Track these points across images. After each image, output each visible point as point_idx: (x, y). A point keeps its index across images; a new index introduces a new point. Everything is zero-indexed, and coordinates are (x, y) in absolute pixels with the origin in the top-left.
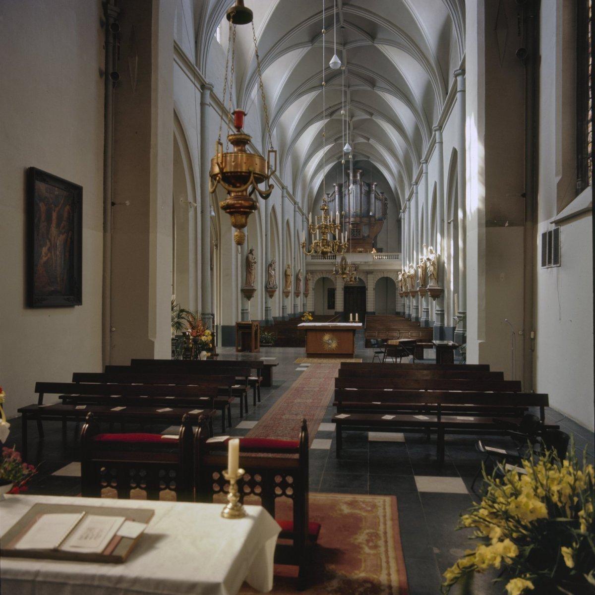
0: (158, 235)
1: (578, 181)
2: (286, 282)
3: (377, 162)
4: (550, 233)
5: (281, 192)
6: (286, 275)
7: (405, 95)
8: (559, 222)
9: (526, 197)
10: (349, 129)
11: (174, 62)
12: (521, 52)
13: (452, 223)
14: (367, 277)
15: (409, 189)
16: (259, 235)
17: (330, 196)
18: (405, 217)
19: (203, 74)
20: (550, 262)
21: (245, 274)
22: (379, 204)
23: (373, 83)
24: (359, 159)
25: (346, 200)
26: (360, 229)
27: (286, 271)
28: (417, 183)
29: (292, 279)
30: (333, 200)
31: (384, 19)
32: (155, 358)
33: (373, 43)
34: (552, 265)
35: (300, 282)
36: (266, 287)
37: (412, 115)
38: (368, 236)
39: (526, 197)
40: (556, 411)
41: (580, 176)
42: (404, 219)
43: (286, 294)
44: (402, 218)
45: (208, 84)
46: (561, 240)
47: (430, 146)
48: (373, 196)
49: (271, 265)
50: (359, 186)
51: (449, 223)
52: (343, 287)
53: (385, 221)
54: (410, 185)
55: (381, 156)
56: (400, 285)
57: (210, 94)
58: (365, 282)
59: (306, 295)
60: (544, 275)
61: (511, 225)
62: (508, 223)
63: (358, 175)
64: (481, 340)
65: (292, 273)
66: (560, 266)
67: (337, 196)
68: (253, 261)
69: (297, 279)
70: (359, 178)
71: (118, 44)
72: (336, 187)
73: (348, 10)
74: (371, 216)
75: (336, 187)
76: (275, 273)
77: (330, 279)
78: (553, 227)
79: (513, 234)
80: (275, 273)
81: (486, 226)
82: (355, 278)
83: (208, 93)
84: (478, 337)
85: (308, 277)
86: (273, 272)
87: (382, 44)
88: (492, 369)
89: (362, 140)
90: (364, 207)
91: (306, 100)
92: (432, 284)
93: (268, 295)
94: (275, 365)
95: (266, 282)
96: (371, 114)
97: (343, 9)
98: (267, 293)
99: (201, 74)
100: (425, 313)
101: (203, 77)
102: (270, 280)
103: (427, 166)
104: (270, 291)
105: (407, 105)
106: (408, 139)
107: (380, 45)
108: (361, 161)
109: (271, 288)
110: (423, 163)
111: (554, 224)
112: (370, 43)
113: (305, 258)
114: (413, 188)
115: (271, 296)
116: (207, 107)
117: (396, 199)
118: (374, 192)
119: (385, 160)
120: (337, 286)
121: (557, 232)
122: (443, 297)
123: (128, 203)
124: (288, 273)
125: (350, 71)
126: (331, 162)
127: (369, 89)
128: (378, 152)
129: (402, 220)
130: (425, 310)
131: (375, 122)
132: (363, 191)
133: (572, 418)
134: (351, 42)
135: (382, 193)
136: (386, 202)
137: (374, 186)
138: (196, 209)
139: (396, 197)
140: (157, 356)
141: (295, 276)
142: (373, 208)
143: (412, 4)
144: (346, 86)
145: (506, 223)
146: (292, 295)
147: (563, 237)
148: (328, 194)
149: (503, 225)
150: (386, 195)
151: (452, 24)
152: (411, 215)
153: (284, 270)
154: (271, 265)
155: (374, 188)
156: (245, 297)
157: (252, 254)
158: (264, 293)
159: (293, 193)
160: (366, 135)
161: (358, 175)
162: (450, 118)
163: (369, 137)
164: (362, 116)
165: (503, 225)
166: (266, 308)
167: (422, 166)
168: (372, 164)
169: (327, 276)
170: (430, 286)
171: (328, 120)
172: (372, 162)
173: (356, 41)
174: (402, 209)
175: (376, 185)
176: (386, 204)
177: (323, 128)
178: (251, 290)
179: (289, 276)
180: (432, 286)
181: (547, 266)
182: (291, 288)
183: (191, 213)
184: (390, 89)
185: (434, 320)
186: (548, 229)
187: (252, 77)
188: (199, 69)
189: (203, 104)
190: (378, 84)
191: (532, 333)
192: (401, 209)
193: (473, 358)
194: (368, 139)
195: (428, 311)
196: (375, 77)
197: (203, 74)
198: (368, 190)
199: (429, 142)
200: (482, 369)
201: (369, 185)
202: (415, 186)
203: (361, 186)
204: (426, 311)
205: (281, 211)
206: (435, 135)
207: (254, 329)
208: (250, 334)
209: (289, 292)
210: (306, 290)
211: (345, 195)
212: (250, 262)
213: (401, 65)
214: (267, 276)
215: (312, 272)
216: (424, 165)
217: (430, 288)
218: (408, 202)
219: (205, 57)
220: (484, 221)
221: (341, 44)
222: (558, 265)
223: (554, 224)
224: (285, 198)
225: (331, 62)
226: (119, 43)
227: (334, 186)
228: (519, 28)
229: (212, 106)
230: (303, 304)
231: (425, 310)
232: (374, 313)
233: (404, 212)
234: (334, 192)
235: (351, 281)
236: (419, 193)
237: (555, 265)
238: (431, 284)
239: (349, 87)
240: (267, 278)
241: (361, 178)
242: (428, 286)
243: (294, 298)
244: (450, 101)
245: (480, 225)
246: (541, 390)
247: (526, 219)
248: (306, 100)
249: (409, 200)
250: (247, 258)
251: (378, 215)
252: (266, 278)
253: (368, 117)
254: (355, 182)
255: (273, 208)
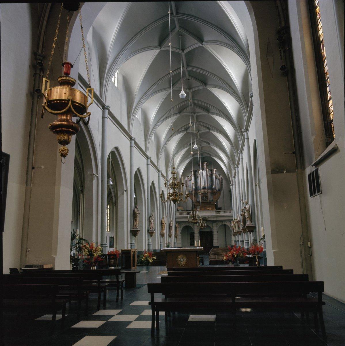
0: (62, 187)
1: (326, 138)
2: (162, 228)
3: (215, 157)
4: (313, 173)
5: (129, 142)
6: (162, 224)
7: (227, 116)
8: (317, 164)
9: (295, 154)
10: (197, 138)
11: (78, 85)
12: (283, 68)
13: (258, 185)
14: (213, 225)
15: (234, 170)
16: (143, 200)
17: (189, 178)
18: (233, 188)
19: (104, 101)
20: (315, 193)
21: (133, 220)
22: (218, 181)
23: (208, 111)
24: (205, 156)
25: (199, 180)
26: (207, 197)
27: (162, 221)
28: (238, 166)
29: (166, 226)
30: (191, 180)
31: (211, 73)
32: (57, 268)
33: (206, 87)
34: (317, 194)
35: (172, 228)
36: (148, 231)
37: (233, 129)
38: (213, 201)
39: (295, 154)
40: (331, 297)
41: (327, 134)
42: (233, 189)
43: (162, 235)
44: (232, 188)
45: (107, 106)
46: (320, 175)
47: (242, 141)
48: (214, 177)
49: (151, 217)
50: (206, 171)
51: (256, 185)
52: (199, 231)
53: (222, 191)
54: (234, 168)
55: (217, 153)
56: (232, 228)
57: (161, 174)
58: (212, 228)
59: (176, 237)
60: (313, 202)
61: (287, 172)
62: (286, 171)
63: (205, 165)
64: (275, 249)
65: (166, 221)
66: (321, 193)
67: (193, 178)
68: (137, 213)
69: (170, 227)
70: (205, 166)
71: (43, 74)
72: (192, 172)
73: (189, 68)
74: (213, 188)
75: (192, 172)
76: (108, 182)
77: (190, 226)
78: (314, 168)
79: (290, 178)
80: (108, 182)
81: (272, 173)
82: (204, 225)
83: (107, 111)
84: (273, 247)
85: (177, 225)
86: (152, 221)
87: (211, 87)
88: (284, 268)
89: (205, 144)
90: (209, 183)
91: (171, 121)
92: (248, 223)
93: (149, 235)
94: (137, 272)
95: (148, 227)
96: (209, 129)
97: (188, 68)
98: (149, 234)
99: (103, 101)
100: (247, 243)
101: (104, 102)
102: (150, 226)
103: (242, 155)
104: (151, 233)
105: (229, 122)
106: (232, 142)
107: (210, 88)
108: (207, 157)
109: (151, 231)
110: (239, 153)
111: (314, 167)
112: (204, 87)
113: (175, 214)
114: (236, 169)
115: (151, 236)
116: (106, 119)
117: (229, 181)
118: (215, 175)
119: (219, 155)
120: (195, 231)
121: (317, 171)
122: (256, 231)
123: (43, 167)
124: (163, 222)
125: (195, 104)
126: (188, 159)
127: (206, 114)
128: (215, 151)
129: (232, 190)
130: (247, 242)
131: (212, 133)
132: (208, 174)
133: (343, 301)
134: (193, 88)
135: (219, 175)
136: (222, 180)
137: (214, 171)
138: (98, 178)
139: (227, 176)
140: (58, 267)
141: (169, 225)
142: (214, 183)
143: (229, 69)
144: (193, 113)
145: (284, 171)
146: (166, 236)
147: (320, 174)
148: (188, 177)
149: (282, 172)
150: (221, 176)
151: (249, 76)
152: (236, 186)
153: (161, 220)
154: (151, 217)
155: (214, 172)
156: (132, 235)
157: (137, 209)
158: (147, 234)
159: (166, 175)
160: (207, 141)
161: (205, 165)
162: (251, 125)
163: (209, 142)
164: (204, 130)
165: (282, 172)
166: (148, 243)
167: (239, 155)
168: (213, 158)
169: (189, 225)
170: (247, 225)
171: (185, 133)
172: (213, 157)
173: (196, 87)
174: (231, 183)
175: (215, 171)
176: (222, 181)
177: (172, 125)
178: (137, 230)
179: (164, 224)
180: (249, 225)
181: (313, 196)
182: (166, 231)
183: (95, 182)
184: (219, 113)
185: (209, 195)
186: (311, 171)
187: (136, 107)
188: (102, 98)
189: (103, 118)
190: (211, 111)
191: (309, 243)
192: (231, 183)
193: (271, 262)
194: (209, 144)
195: (249, 242)
196: (208, 106)
197: (104, 101)
198: (211, 173)
199: (242, 139)
200: (277, 269)
201: (212, 171)
202: (236, 168)
203: (207, 171)
204: (247, 242)
205: (158, 185)
206: (244, 134)
207: (132, 254)
208: (130, 257)
209: (164, 234)
210: (176, 233)
211: (198, 177)
212: (135, 213)
213: (222, 98)
214: (149, 223)
215: (180, 223)
216: (240, 154)
217: (247, 226)
218: (234, 179)
219: (106, 90)
220: (270, 170)
221: (188, 89)
222: (320, 193)
223: (314, 167)
224: (133, 148)
225: (180, 94)
226: (43, 74)
227: (191, 172)
228: (281, 55)
229: (109, 118)
230: (175, 242)
231: (247, 242)
232: (218, 247)
233: (232, 185)
234: (192, 175)
235: (202, 226)
236: (239, 171)
237: (318, 194)
238: (248, 223)
239: (195, 113)
240: (149, 225)
241: (206, 167)
242: (246, 225)
243: (168, 238)
244: (250, 113)
245: (267, 173)
246: (318, 278)
247: (297, 167)
248: (171, 121)
249: (235, 177)
250: (134, 211)
251: (218, 188)
252: (148, 224)
253: (208, 130)
254: (203, 169)
255: (153, 183)
